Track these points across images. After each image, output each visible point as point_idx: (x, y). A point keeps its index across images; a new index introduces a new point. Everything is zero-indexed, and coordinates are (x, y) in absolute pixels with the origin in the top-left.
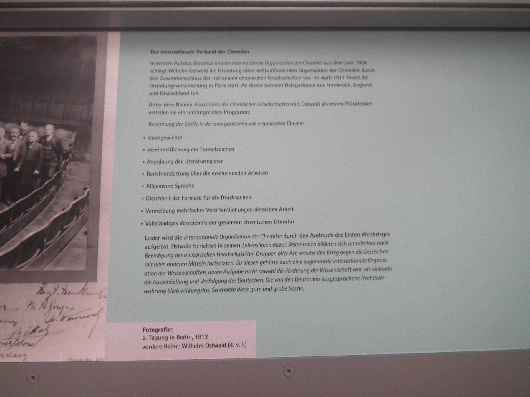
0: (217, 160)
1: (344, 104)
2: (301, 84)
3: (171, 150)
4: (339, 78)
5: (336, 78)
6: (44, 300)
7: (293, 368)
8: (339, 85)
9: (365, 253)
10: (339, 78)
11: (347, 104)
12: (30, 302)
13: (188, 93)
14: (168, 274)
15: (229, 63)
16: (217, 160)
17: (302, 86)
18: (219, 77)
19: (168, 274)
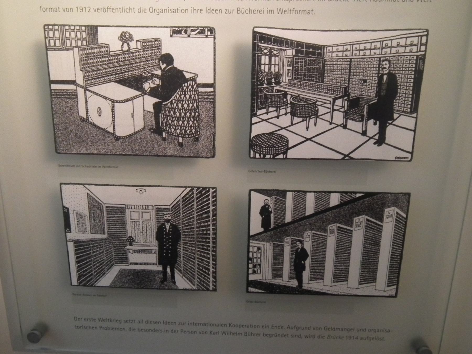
0: (92, 319)
1: (98, 328)
2: (207, 324)
3: (252, 326)
4: (352, 338)
5: (348, 337)
6: (109, 128)
7: (147, 232)
8: (112, 321)
9: (238, 13)
10: (352, 338)
11: (101, 329)
12: (251, 289)
13: (315, 336)
14: (278, 13)
15: (323, 337)
16: (92, 319)
17: (208, 325)
18: (251, 325)
19: (278, 13)
